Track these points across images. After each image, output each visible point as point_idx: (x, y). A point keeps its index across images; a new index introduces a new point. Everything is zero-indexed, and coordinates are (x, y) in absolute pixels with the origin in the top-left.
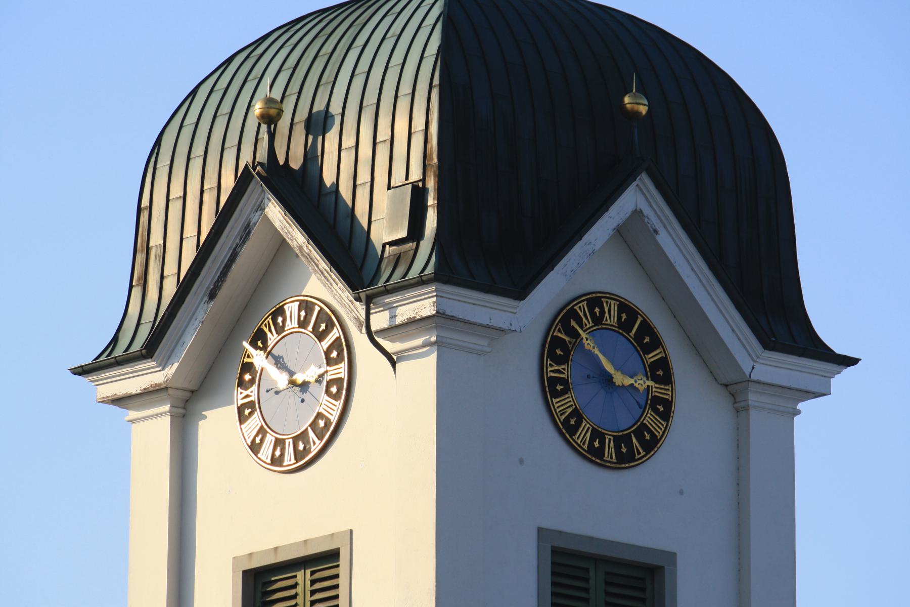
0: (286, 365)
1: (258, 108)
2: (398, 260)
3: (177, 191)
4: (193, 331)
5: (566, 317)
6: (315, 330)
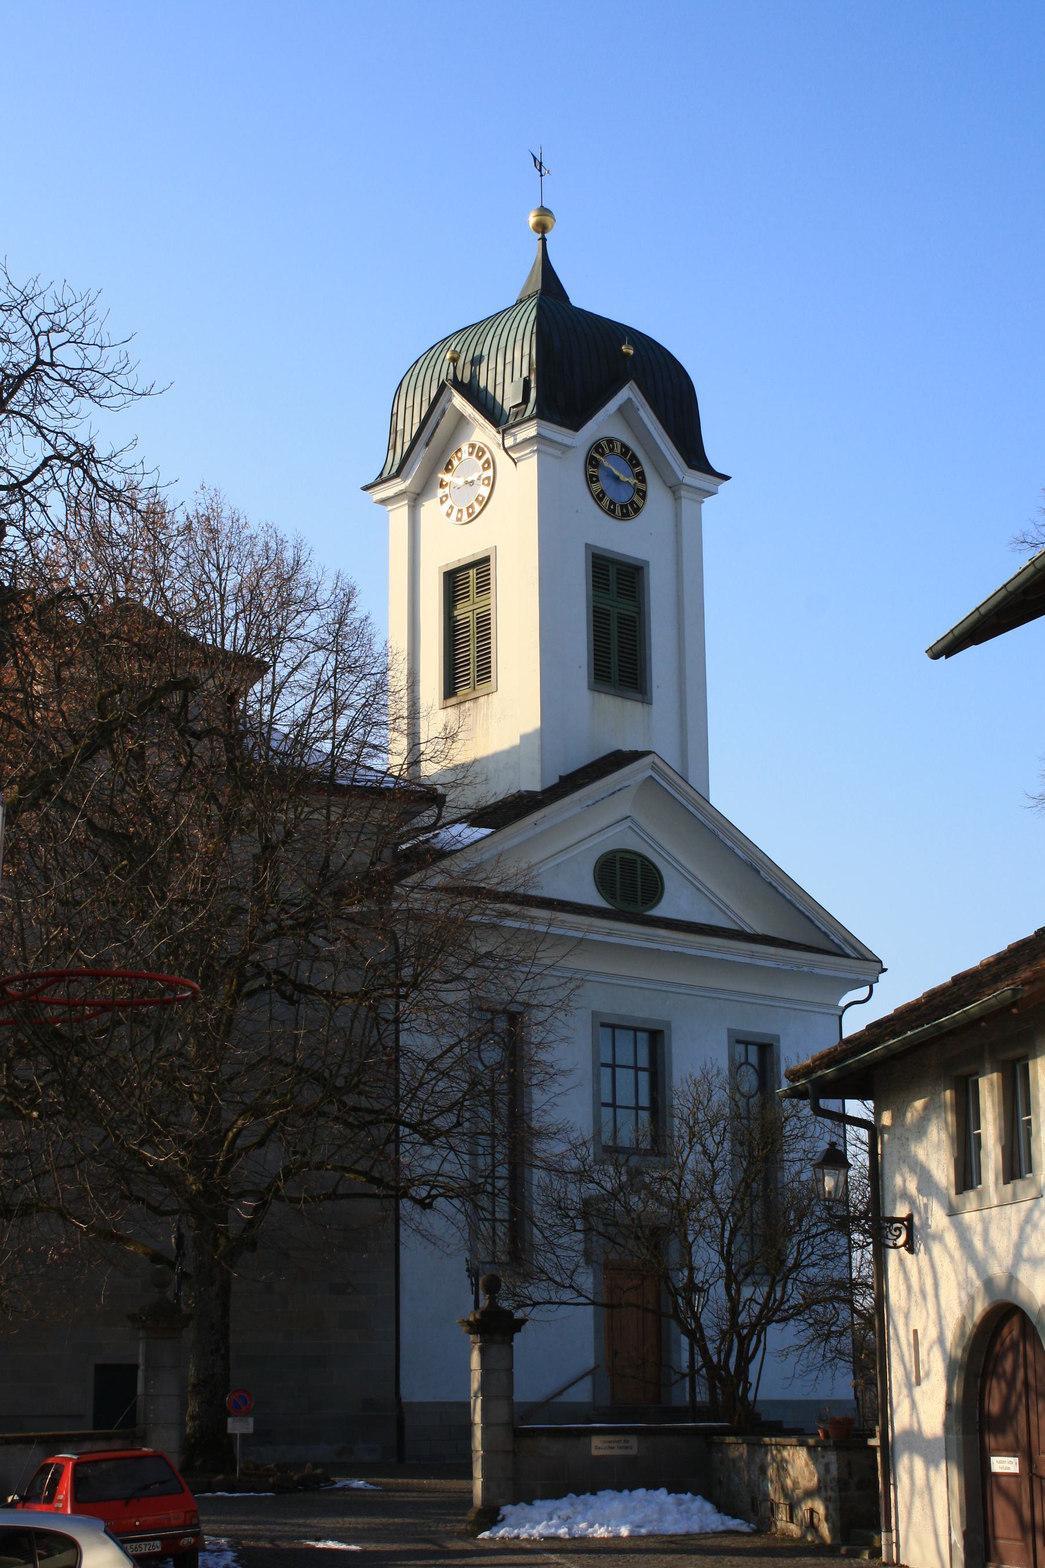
0: (463, 473)
1: (448, 356)
2: (517, 414)
3: (409, 403)
5: (597, 447)
6: (477, 456)
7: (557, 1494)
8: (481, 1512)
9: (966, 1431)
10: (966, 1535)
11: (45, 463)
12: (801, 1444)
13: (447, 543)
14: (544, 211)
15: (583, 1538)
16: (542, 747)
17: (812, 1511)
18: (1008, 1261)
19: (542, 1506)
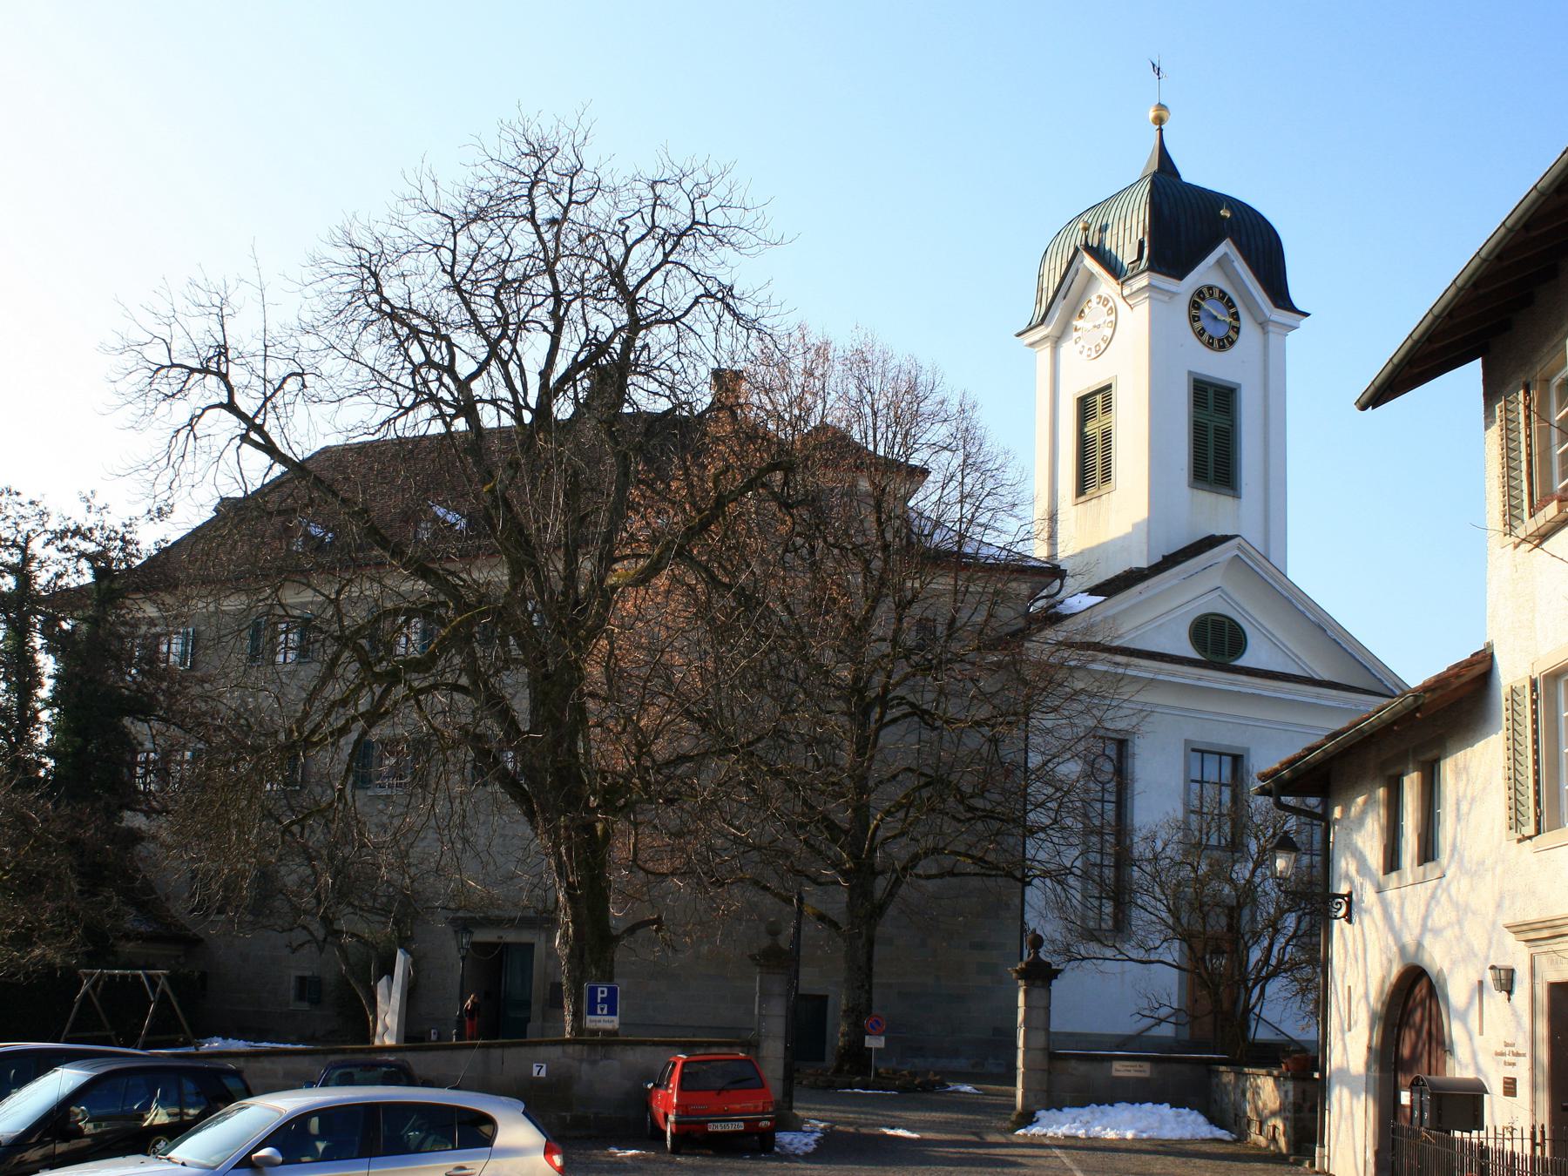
0: (1094, 312)
4: (1060, 306)
5: (1199, 293)
7: (1082, 1103)
8: (1021, 1115)
9: (1382, 1069)
10: (1377, 1154)
11: (696, 301)
12: (1269, 1074)
13: (1080, 377)
14: (1161, 107)
15: (1096, 1139)
16: (1149, 532)
17: (1275, 1127)
18: (1416, 931)
19: (1069, 1112)
